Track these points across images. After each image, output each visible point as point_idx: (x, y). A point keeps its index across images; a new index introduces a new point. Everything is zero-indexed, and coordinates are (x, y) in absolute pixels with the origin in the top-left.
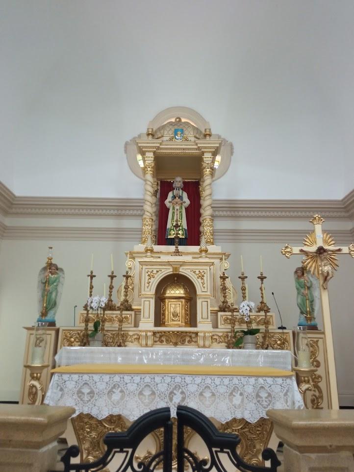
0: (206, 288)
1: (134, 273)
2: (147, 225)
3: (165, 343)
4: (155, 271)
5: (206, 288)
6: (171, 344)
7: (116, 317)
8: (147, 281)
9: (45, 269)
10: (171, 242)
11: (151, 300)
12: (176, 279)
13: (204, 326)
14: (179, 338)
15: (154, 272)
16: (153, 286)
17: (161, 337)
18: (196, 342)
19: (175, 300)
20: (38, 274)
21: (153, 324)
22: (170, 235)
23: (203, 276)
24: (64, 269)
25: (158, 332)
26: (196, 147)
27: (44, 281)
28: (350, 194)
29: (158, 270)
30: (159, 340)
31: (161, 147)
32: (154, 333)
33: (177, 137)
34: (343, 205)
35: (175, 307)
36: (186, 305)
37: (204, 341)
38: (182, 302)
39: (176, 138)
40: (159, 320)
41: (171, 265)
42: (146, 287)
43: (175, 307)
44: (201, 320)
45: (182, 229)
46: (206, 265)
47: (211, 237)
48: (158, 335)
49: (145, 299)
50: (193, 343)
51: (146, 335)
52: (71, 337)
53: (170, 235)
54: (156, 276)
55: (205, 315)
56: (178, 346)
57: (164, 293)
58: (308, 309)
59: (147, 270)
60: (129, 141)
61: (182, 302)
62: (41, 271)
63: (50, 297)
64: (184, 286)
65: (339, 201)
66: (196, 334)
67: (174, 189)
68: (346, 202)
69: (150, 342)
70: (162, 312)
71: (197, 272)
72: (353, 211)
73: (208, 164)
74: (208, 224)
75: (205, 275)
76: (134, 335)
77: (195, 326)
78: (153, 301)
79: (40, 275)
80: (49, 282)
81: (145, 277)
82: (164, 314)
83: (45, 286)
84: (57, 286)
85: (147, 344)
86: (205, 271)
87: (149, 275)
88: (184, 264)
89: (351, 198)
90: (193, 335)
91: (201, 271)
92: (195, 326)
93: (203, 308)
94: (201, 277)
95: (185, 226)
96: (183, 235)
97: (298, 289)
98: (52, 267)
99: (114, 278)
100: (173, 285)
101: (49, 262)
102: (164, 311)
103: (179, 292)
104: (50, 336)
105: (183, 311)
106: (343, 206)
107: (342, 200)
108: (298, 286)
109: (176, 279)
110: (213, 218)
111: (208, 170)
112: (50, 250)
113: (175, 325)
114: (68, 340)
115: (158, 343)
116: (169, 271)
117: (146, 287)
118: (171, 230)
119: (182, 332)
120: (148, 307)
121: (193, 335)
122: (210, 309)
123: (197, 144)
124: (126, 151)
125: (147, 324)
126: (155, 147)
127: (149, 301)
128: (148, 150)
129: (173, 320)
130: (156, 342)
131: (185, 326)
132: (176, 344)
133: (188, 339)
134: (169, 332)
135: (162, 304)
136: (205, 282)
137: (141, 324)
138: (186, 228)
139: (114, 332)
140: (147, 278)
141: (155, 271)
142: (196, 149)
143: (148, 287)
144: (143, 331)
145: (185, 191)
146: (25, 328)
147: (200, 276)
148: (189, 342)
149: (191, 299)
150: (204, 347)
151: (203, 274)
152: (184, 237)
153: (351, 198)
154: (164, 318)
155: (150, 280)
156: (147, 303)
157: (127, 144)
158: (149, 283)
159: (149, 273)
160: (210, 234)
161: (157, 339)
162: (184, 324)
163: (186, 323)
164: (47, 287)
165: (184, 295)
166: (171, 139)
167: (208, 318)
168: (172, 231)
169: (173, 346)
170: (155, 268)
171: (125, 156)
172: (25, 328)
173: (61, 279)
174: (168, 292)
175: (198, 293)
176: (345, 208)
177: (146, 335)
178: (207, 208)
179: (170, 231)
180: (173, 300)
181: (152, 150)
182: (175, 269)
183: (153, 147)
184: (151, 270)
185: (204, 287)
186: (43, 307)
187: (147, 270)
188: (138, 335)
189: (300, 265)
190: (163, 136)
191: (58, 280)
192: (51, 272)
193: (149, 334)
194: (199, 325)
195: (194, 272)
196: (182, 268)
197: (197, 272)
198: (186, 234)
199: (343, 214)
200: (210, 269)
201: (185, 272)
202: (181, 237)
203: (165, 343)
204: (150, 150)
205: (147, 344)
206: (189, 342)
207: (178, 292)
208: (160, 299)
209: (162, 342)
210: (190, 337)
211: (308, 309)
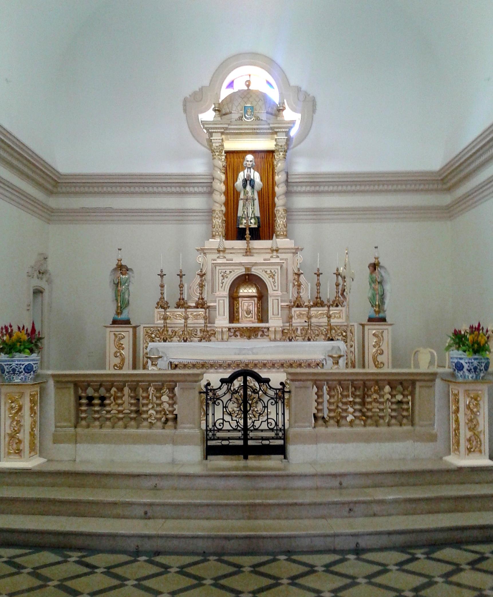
0: (277, 287)
1: (208, 269)
2: (217, 218)
3: (239, 337)
4: (228, 272)
5: (277, 287)
6: (245, 338)
7: (191, 314)
8: (220, 282)
9: (115, 270)
10: (240, 234)
11: (225, 299)
12: (248, 278)
13: (275, 322)
14: (251, 333)
15: (227, 273)
16: (226, 286)
17: (235, 332)
18: (268, 336)
19: (248, 299)
20: (109, 274)
21: (228, 321)
22: (242, 224)
23: (274, 275)
24: (133, 269)
25: (233, 328)
26: (267, 127)
27: (116, 282)
28: (489, 128)
29: (231, 270)
30: (234, 335)
31: (230, 127)
32: (229, 329)
33: (246, 115)
34: (440, 176)
35: (247, 306)
36: (258, 303)
37: (275, 335)
38: (254, 301)
39: (245, 117)
40: (233, 317)
41: (243, 266)
42: (220, 287)
43: (247, 306)
44: (272, 316)
45: (254, 217)
46: (277, 265)
47: (285, 229)
48: (232, 330)
49: (220, 299)
50: (265, 337)
51: (222, 331)
52: (152, 334)
53: (242, 224)
54: (229, 276)
55: (276, 312)
56: (251, 340)
57: (237, 292)
58: (377, 303)
59: (220, 271)
60: (188, 96)
61: (254, 301)
62: (112, 272)
63: (123, 297)
64: (256, 285)
65: (432, 173)
66: (268, 329)
67: (245, 169)
68: (454, 164)
69: (225, 337)
70: (235, 310)
71: (269, 272)
72: (491, 151)
73: (281, 146)
74: (282, 216)
75: (276, 275)
76: (210, 330)
77: (267, 322)
78: (227, 301)
79: (111, 275)
80: (121, 282)
81: (218, 278)
82: (238, 312)
83: (118, 286)
84: (128, 286)
85: (222, 339)
86: (276, 270)
87: (222, 276)
88: (256, 264)
89: (489, 134)
90: (266, 330)
91: (273, 271)
92: (267, 322)
93: (273, 305)
94: (272, 276)
95: (258, 214)
96: (255, 224)
97: (370, 284)
98: (121, 268)
99: (183, 277)
100: (245, 284)
101: (119, 264)
102: (238, 309)
103: (252, 291)
104: (386, 331)
105: (256, 309)
106: (440, 178)
107: (439, 171)
108: (370, 280)
109: (248, 278)
110: (288, 193)
111: (281, 153)
112: (120, 251)
113: (247, 322)
114: (150, 336)
115: (233, 337)
116: (242, 271)
117: (220, 287)
118: (242, 218)
119: (255, 328)
120: (222, 306)
121: (266, 330)
122: (280, 304)
123: (269, 124)
124: (185, 111)
125: (222, 321)
126: (223, 128)
127: (224, 300)
128: (215, 131)
129: (246, 317)
130: (231, 336)
131: (258, 322)
132: (249, 338)
133: (260, 333)
134: (243, 328)
135: (235, 302)
136: (276, 281)
137: (216, 322)
138: (259, 215)
139: (191, 329)
140: (221, 278)
141: (228, 272)
142: (269, 129)
143: (222, 287)
144: (219, 328)
145: (258, 172)
146: (33, 324)
147: (271, 276)
148: (262, 336)
149: (262, 297)
150: (275, 340)
151: (274, 273)
152: (256, 226)
153: (489, 134)
154: (238, 315)
155: (223, 281)
156: (221, 302)
157: (185, 101)
158: (223, 283)
159: (223, 274)
160: (283, 226)
161: (232, 334)
162: (257, 321)
163: (258, 319)
164: (119, 288)
165: (256, 294)
166: (241, 118)
167: (278, 314)
168: (243, 219)
169: (246, 340)
170: (228, 269)
171: (184, 116)
172: (33, 324)
173: (132, 279)
174: (241, 291)
175: (269, 292)
176: (442, 180)
177: (222, 331)
178: (281, 197)
179: (242, 220)
180: (246, 299)
181: (220, 131)
182: (247, 269)
183: (221, 128)
184: (224, 271)
185: (275, 286)
186: (118, 307)
187: (220, 271)
188: (214, 331)
189: (373, 261)
190: (231, 113)
191: (128, 281)
192: (121, 273)
193: (224, 330)
194: (270, 321)
195: (266, 272)
196: (254, 268)
197: (269, 272)
198: (259, 222)
199: (440, 186)
200: (274, 282)
201: (257, 271)
202: (253, 226)
203: (239, 337)
204: (218, 131)
205: (222, 339)
206: (262, 336)
207: (250, 291)
208: (233, 298)
209: (236, 336)
210: (263, 331)
211: (377, 303)
